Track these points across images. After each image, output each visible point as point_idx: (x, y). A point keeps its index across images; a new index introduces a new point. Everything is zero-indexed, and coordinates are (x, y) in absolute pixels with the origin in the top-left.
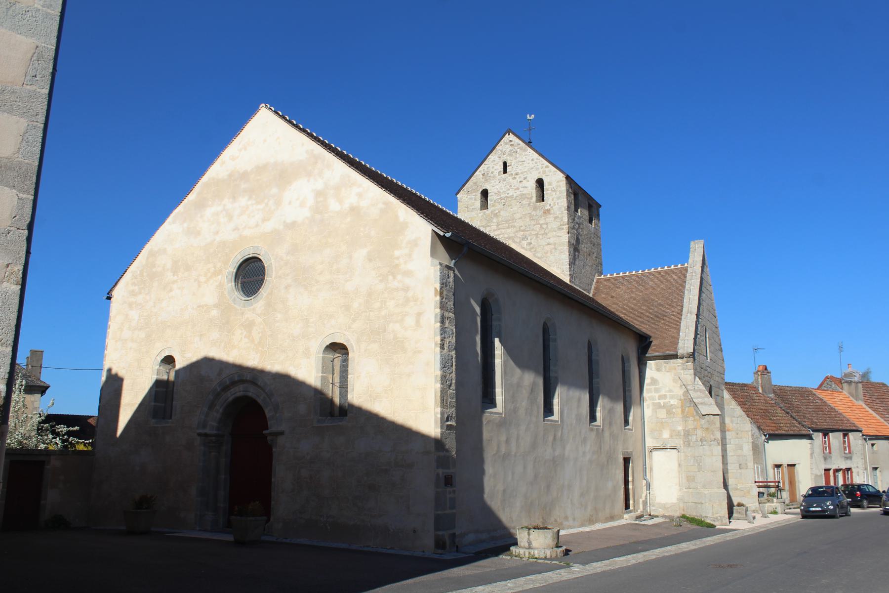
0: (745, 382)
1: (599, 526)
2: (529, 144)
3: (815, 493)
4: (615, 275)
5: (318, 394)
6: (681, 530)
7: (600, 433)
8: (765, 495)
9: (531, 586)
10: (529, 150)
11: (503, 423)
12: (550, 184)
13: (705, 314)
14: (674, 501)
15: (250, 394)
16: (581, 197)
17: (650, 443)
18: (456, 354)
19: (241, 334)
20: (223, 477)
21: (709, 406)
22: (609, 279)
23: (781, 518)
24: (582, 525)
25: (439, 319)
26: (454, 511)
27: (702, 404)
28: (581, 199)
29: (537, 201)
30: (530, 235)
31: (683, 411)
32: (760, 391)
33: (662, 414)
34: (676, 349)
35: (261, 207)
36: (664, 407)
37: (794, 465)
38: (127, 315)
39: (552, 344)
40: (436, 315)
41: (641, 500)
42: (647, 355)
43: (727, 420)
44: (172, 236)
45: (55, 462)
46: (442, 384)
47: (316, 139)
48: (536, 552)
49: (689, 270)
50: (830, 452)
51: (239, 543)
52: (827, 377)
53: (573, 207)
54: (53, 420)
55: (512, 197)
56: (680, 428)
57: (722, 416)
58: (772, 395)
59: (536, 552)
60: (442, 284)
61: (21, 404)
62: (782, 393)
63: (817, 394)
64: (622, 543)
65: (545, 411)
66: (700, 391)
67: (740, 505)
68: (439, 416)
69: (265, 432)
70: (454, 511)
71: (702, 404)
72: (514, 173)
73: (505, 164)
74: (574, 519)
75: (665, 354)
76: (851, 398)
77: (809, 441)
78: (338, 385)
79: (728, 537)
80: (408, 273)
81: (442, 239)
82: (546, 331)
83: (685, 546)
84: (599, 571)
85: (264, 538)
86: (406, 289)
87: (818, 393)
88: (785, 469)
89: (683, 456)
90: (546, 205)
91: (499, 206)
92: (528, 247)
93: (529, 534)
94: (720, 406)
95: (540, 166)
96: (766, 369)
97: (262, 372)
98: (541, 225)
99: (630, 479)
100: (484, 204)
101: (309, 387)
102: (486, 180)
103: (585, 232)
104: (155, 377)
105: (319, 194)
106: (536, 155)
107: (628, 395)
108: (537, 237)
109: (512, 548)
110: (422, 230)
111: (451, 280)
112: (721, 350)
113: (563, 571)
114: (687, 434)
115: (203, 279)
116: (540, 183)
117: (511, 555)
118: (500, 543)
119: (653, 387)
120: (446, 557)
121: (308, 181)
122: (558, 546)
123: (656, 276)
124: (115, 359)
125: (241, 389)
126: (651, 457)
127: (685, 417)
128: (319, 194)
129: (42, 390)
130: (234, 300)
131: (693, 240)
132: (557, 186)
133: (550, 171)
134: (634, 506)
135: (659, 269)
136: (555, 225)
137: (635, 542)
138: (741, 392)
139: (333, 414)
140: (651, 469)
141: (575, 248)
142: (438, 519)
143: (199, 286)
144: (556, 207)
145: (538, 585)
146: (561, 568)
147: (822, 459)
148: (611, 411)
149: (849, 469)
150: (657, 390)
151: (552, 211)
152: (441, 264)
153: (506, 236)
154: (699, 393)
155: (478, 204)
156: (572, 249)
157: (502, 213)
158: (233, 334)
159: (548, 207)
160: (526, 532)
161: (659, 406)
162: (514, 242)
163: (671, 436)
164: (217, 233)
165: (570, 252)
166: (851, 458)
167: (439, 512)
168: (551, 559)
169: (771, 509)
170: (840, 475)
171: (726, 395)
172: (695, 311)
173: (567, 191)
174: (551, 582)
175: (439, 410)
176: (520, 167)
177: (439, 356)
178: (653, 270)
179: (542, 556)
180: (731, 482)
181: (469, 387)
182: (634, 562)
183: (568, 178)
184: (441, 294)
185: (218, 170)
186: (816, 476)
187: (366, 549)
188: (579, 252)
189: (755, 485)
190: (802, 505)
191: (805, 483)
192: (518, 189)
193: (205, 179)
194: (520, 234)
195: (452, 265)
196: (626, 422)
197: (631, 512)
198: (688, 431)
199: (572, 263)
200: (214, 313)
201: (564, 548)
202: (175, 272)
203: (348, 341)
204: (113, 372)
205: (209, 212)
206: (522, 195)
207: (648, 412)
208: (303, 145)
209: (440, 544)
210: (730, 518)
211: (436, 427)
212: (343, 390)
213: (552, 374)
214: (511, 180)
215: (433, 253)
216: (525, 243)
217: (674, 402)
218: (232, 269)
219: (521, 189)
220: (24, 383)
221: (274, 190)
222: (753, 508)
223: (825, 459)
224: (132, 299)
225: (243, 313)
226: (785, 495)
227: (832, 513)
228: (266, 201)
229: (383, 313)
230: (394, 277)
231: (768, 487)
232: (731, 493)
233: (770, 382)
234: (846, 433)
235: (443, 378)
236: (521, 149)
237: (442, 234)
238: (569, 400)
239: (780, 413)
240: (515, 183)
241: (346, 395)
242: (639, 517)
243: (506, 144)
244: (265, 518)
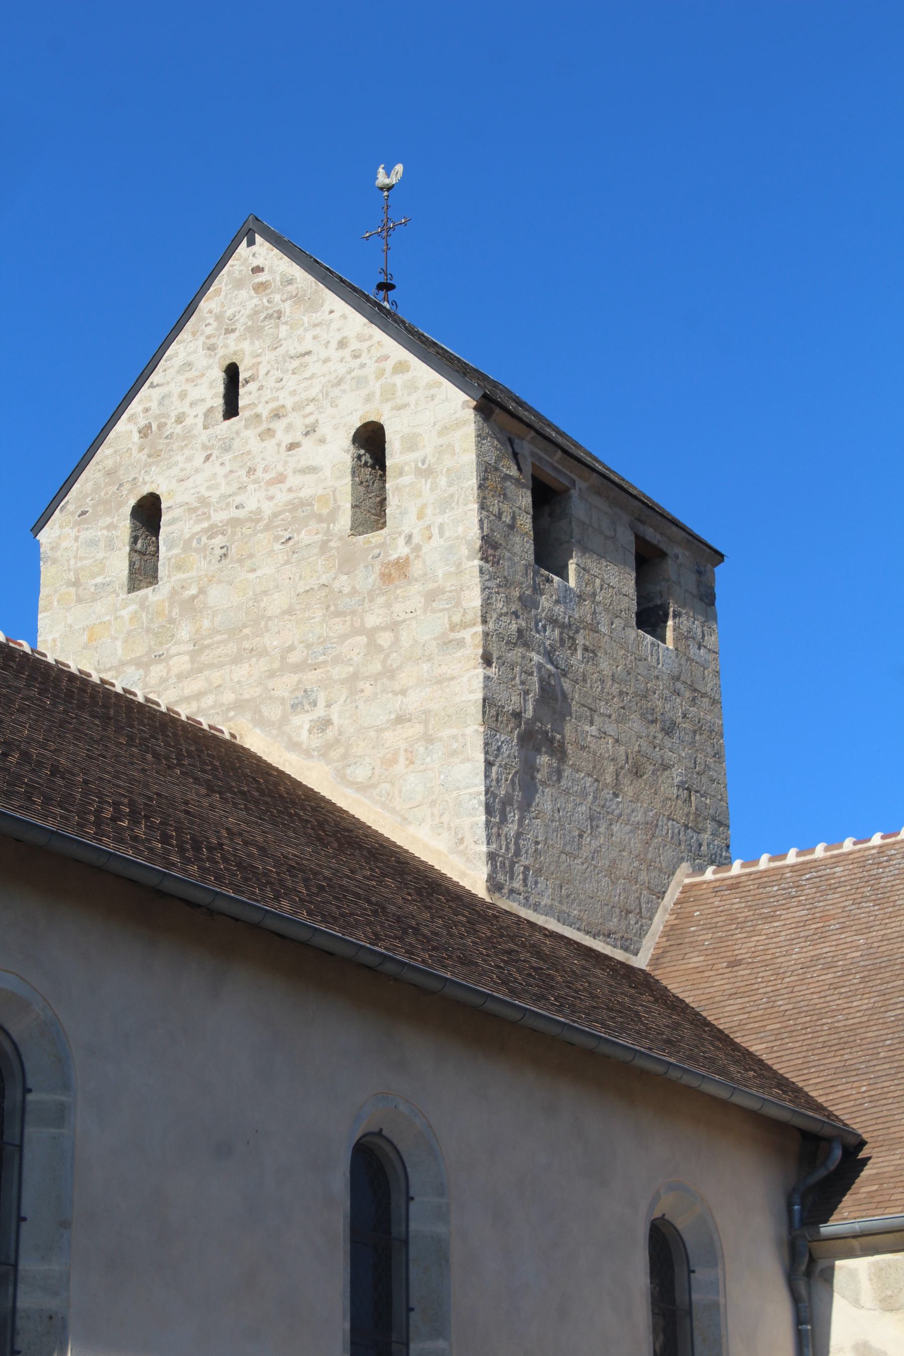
12: (411, 442)
16: (581, 506)
22: (735, 885)
28: (550, 491)
53: (523, 546)
55: (255, 517)
72: (264, 410)
73: (232, 373)
90: (392, 542)
91: (200, 566)
92: (316, 741)
95: (372, 367)
98: (371, 634)
102: (155, 454)
116: (371, 440)
132: (441, 450)
133: (411, 387)
136: (426, 628)
144: (432, 550)
151: (416, 568)
153: (228, 697)
155: (119, 564)
156: (510, 746)
157: (215, 595)
159: (401, 550)
162: (260, 721)
173: (487, 475)
176: (291, 382)
183: (493, 405)
188: (559, 752)
192: (281, 479)
194: (284, 686)
199: (496, 808)
214: (254, 444)
216: (302, 722)
236: (297, 299)
240: (268, 453)
241: (851, 1254)
243: (239, 284)
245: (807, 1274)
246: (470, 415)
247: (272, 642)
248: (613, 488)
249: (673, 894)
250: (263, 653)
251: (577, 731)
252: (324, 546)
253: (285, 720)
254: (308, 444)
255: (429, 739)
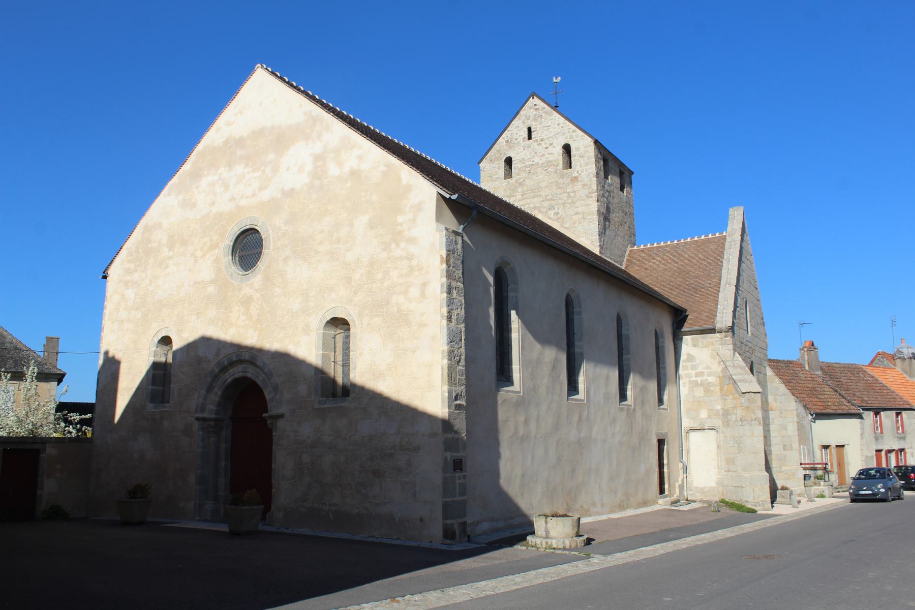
0: (790, 359)
1: (630, 512)
2: (556, 108)
3: (865, 474)
4: (649, 246)
5: (319, 373)
6: (719, 516)
7: (631, 413)
8: (812, 478)
9: (541, 581)
10: (555, 114)
11: (521, 403)
12: (578, 149)
13: (744, 285)
14: (713, 484)
15: (249, 375)
16: (611, 164)
17: (686, 423)
18: (465, 327)
19: (239, 311)
20: (223, 463)
21: (750, 384)
22: (642, 250)
23: (828, 502)
24: (612, 512)
25: (445, 289)
26: (464, 498)
27: (741, 381)
28: (610, 164)
29: (564, 168)
30: (557, 204)
31: (721, 389)
32: (807, 368)
33: (699, 392)
34: (713, 323)
35: (257, 174)
36: (702, 384)
37: (843, 446)
38: (123, 295)
39: (576, 317)
40: (442, 285)
41: (677, 484)
42: (683, 330)
43: (771, 399)
44: (167, 209)
45: (50, 450)
46: (450, 360)
47: (312, 98)
48: (554, 541)
49: (728, 239)
50: (882, 432)
51: (234, 534)
52: (879, 354)
53: (602, 173)
54: (62, 407)
55: (537, 164)
56: (719, 407)
57: (764, 394)
58: (819, 373)
59: (554, 541)
60: (448, 251)
61: (33, 392)
62: (830, 371)
63: (868, 371)
64: (652, 531)
65: (568, 390)
66: (740, 367)
67: (784, 488)
68: (446, 394)
69: (265, 415)
70: (464, 498)
71: (741, 381)
72: (539, 139)
73: (529, 129)
74: (603, 505)
75: (702, 328)
76: (905, 375)
77: (859, 421)
78: (341, 363)
79: (769, 523)
80: (412, 240)
81: (448, 202)
82: (569, 304)
83: (659, 549)
84: (620, 562)
85: (261, 527)
86: (410, 257)
87: (869, 370)
88: (834, 451)
89: (721, 436)
91: (523, 175)
92: (555, 217)
93: (546, 523)
94: (762, 383)
95: (566, 131)
96: (813, 345)
97: (260, 351)
98: (568, 193)
99: (665, 461)
100: (508, 174)
101: (309, 365)
103: (616, 201)
104: (152, 360)
105: (318, 158)
106: (562, 119)
107: (662, 374)
108: (564, 207)
109: (529, 538)
110: (426, 192)
111: (459, 246)
112: (763, 324)
113: (580, 564)
114: (726, 413)
115: (199, 254)
116: (567, 148)
117: (527, 545)
118: (518, 532)
119: (689, 364)
120: (456, 548)
121: (307, 144)
122: (578, 535)
123: (693, 246)
124: (112, 341)
125: (240, 370)
126: (687, 439)
127: (724, 396)
128: (318, 158)
129: (59, 378)
130: (231, 275)
131: (733, 206)
132: (585, 152)
133: (577, 136)
134: (670, 491)
135: (696, 238)
137: (667, 530)
138: (785, 369)
139: (335, 394)
140: (688, 451)
141: (605, 217)
142: (446, 506)
143: (196, 261)
144: (584, 174)
145: (549, 579)
146: (579, 559)
147: (874, 440)
148: (643, 390)
149: (902, 450)
150: (694, 367)
151: (580, 179)
152: (447, 229)
153: (532, 206)
154: (738, 370)
155: (502, 172)
156: (602, 219)
157: (527, 181)
158: (231, 312)
159: (576, 174)
160: (543, 519)
161: (696, 384)
162: (540, 212)
163: (709, 416)
164: (213, 204)
165: (599, 222)
166: (904, 438)
167: (449, 500)
168: (570, 549)
169: (818, 493)
170: (893, 456)
171: (769, 372)
172: (734, 282)
173: (596, 156)
174: (564, 575)
175: (446, 388)
176: (546, 132)
177: (446, 330)
178: (689, 239)
179: (561, 546)
180: (774, 465)
181: (484, 362)
182: (662, 552)
184: (448, 261)
185: (214, 136)
186: (867, 457)
187: (370, 539)
188: (609, 221)
189: (800, 467)
190: (850, 488)
191: (855, 464)
192: (544, 155)
193: (200, 147)
194: (546, 204)
195: (460, 231)
196: (661, 401)
197: (666, 497)
198: (727, 410)
199: (602, 233)
200: (211, 289)
201: (586, 537)
202: (171, 247)
203: (350, 315)
204: (110, 355)
205: (204, 182)
206: (547, 162)
207: (684, 390)
208: (301, 106)
209: (449, 534)
210: (772, 502)
211: (443, 407)
212: (346, 368)
213: (577, 350)
214: (536, 147)
215: (439, 217)
216: (551, 213)
217: (711, 379)
218: (229, 242)
219: (547, 156)
220: (36, 370)
221: (272, 156)
222: (799, 492)
223: (877, 439)
224: (128, 278)
225: (240, 289)
226: (834, 478)
227: (884, 497)
228: (263, 168)
229: (386, 284)
230: (398, 245)
231: (815, 469)
232: (775, 476)
233: (817, 359)
234: (899, 411)
235: (451, 354)
236: (546, 113)
237: (447, 196)
238: (597, 378)
239: (828, 392)
242: (675, 502)
243: (531, 108)
244: (262, 507)
245: (677, 338)
246: (593, 144)
247: (543, 194)
248: (616, 159)
249: (628, 252)
250: (540, 196)
251: (613, 216)
252: (556, 172)
253: (547, 212)
254: (550, 148)
255: (584, 218)
